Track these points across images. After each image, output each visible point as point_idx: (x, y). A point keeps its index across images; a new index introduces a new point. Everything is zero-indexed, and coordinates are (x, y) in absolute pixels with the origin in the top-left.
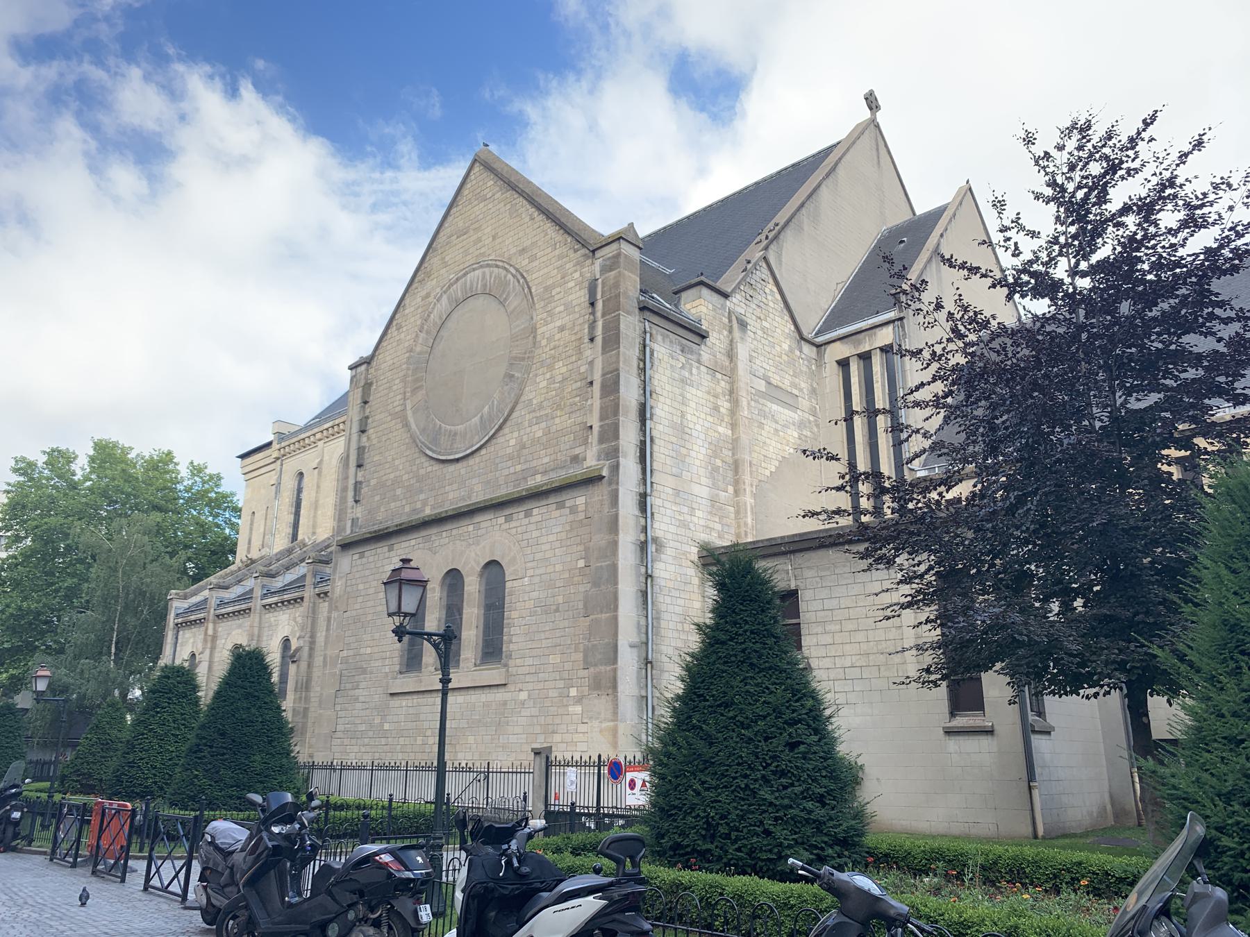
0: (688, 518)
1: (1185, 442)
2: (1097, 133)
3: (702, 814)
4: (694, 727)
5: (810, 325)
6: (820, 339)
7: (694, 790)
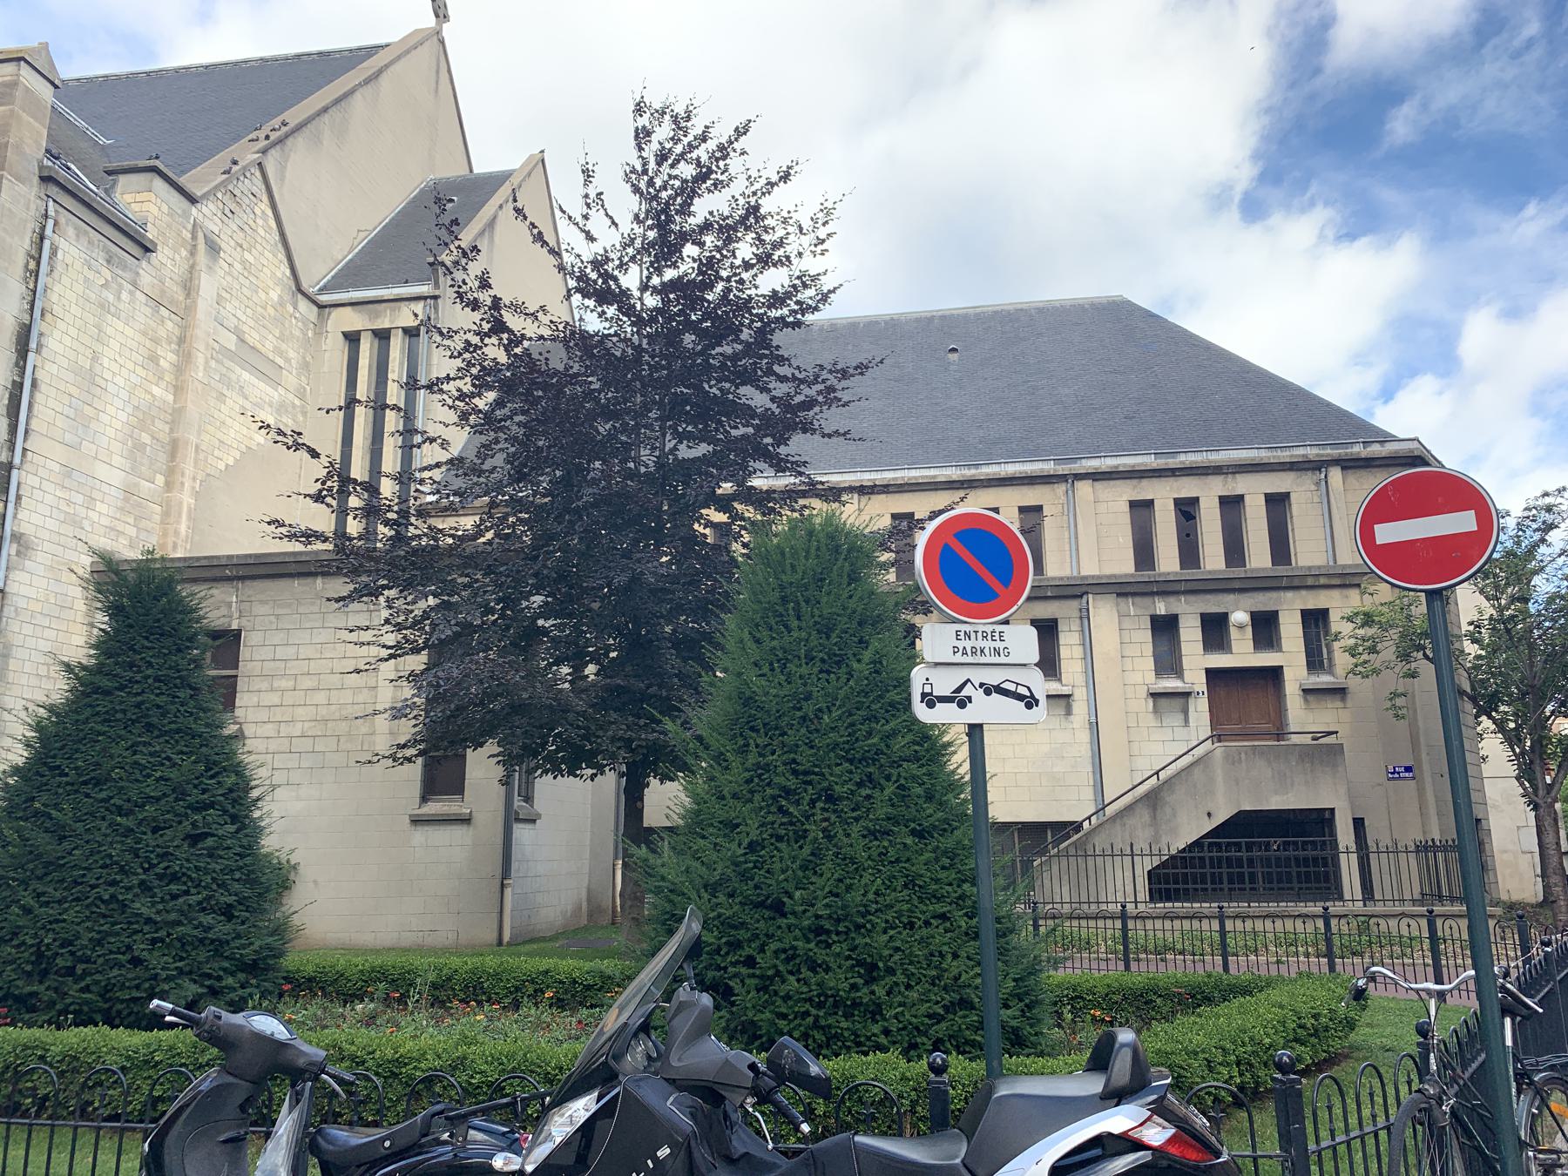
0: (82, 512)
1: (724, 504)
2: (696, 128)
3: (30, 942)
4: (36, 813)
5: (316, 274)
6: (324, 298)
7: (23, 908)
